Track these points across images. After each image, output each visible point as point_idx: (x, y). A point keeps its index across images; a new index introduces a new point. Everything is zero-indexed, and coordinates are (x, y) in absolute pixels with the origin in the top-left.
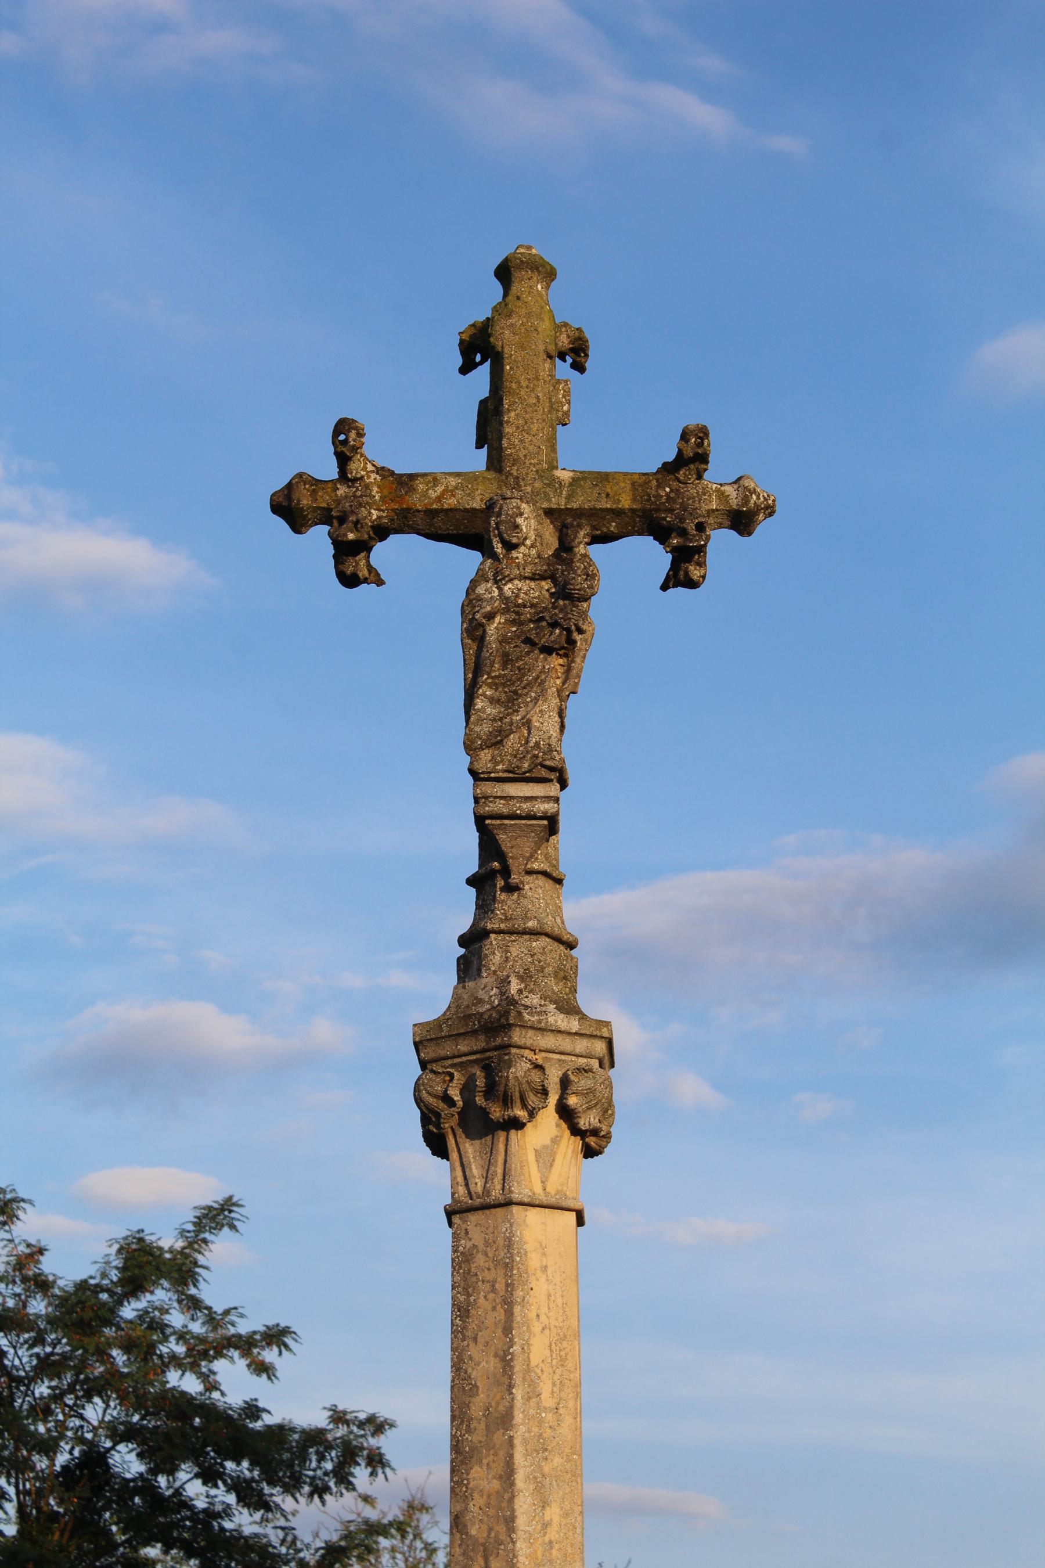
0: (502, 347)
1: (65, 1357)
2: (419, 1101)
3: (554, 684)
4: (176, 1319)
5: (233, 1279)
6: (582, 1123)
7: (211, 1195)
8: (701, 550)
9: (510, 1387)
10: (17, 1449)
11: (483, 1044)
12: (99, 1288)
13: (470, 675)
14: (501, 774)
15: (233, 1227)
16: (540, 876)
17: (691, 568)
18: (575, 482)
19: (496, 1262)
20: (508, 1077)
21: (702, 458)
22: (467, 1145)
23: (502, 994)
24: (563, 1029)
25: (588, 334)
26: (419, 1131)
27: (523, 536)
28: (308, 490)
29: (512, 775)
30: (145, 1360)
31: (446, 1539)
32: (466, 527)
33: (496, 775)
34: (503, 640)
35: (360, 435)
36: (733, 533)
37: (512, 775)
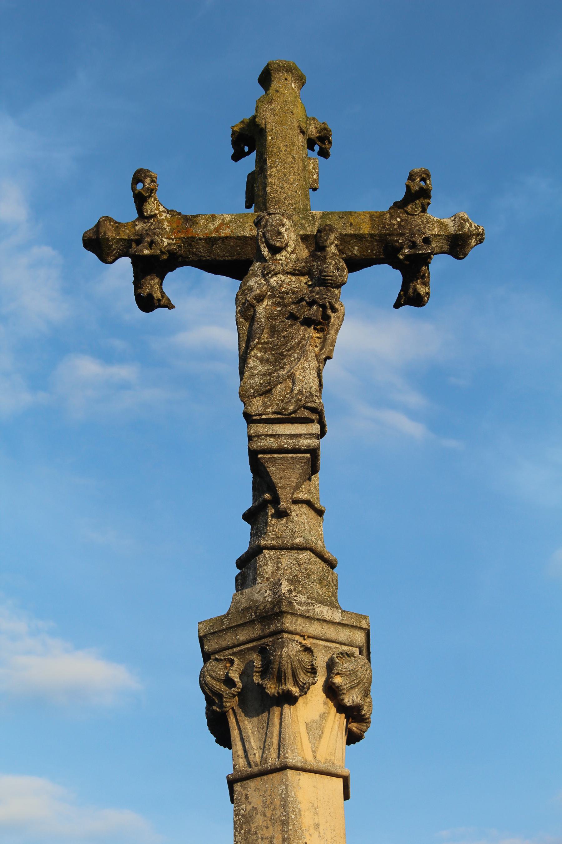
0: (265, 125)
2: (203, 685)
3: (313, 351)
6: (346, 701)
11: (259, 632)
13: (244, 345)
14: (271, 416)
16: (304, 505)
17: (419, 286)
19: (273, 820)
20: (281, 655)
21: (425, 193)
22: (246, 722)
23: (274, 594)
24: (328, 619)
25: (330, 127)
28: (112, 226)
29: (279, 416)
32: (239, 254)
33: (267, 417)
34: (271, 317)
37: (279, 416)
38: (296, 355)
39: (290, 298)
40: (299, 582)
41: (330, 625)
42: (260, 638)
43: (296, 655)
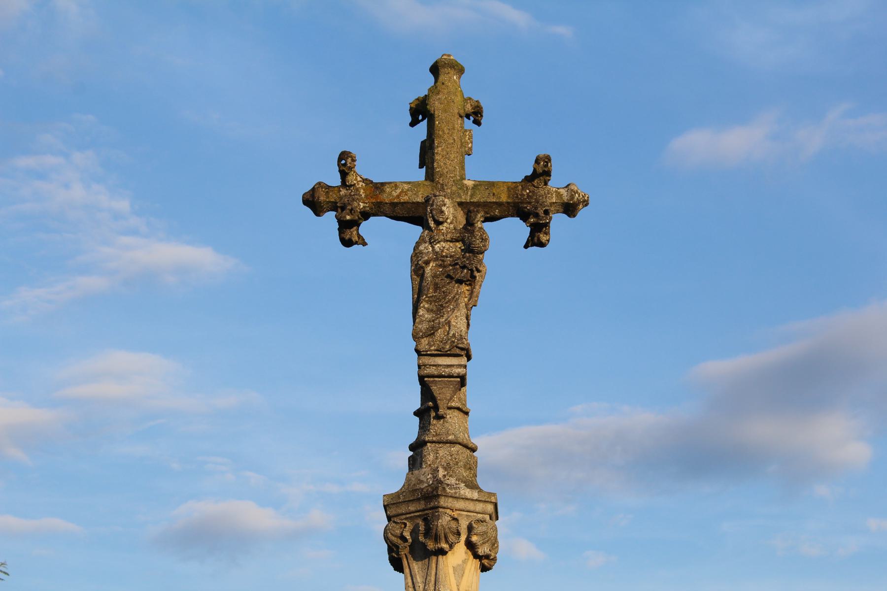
2: (386, 539)
3: (463, 301)
17: (541, 235)
21: (548, 173)
25: (482, 104)
34: (435, 276)
42: (423, 510)
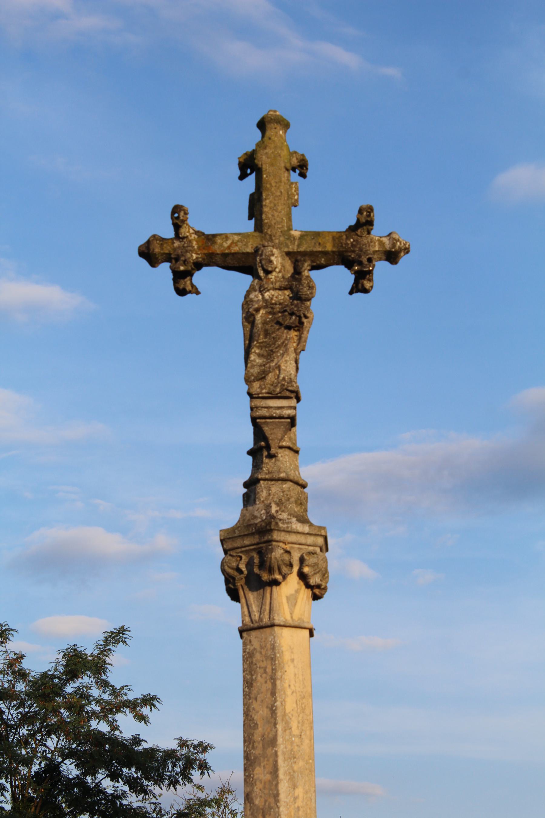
0: (262, 165)
1: (35, 713)
2: (223, 571)
3: (292, 346)
4: (95, 692)
5: (122, 669)
7: (113, 626)
8: (370, 272)
9: (275, 724)
10: (11, 763)
12: (53, 676)
13: (247, 342)
14: (265, 395)
15: (124, 642)
17: (365, 282)
18: (302, 237)
19: (267, 657)
21: (370, 223)
23: (267, 513)
25: (308, 157)
26: (224, 587)
27: (274, 266)
30: (79, 714)
31: (242, 808)
34: (265, 323)
35: (186, 213)
36: (387, 263)
38: (281, 352)
39: (278, 308)
40: (283, 504)
41: (301, 535)
42: (258, 544)
43: (280, 557)
